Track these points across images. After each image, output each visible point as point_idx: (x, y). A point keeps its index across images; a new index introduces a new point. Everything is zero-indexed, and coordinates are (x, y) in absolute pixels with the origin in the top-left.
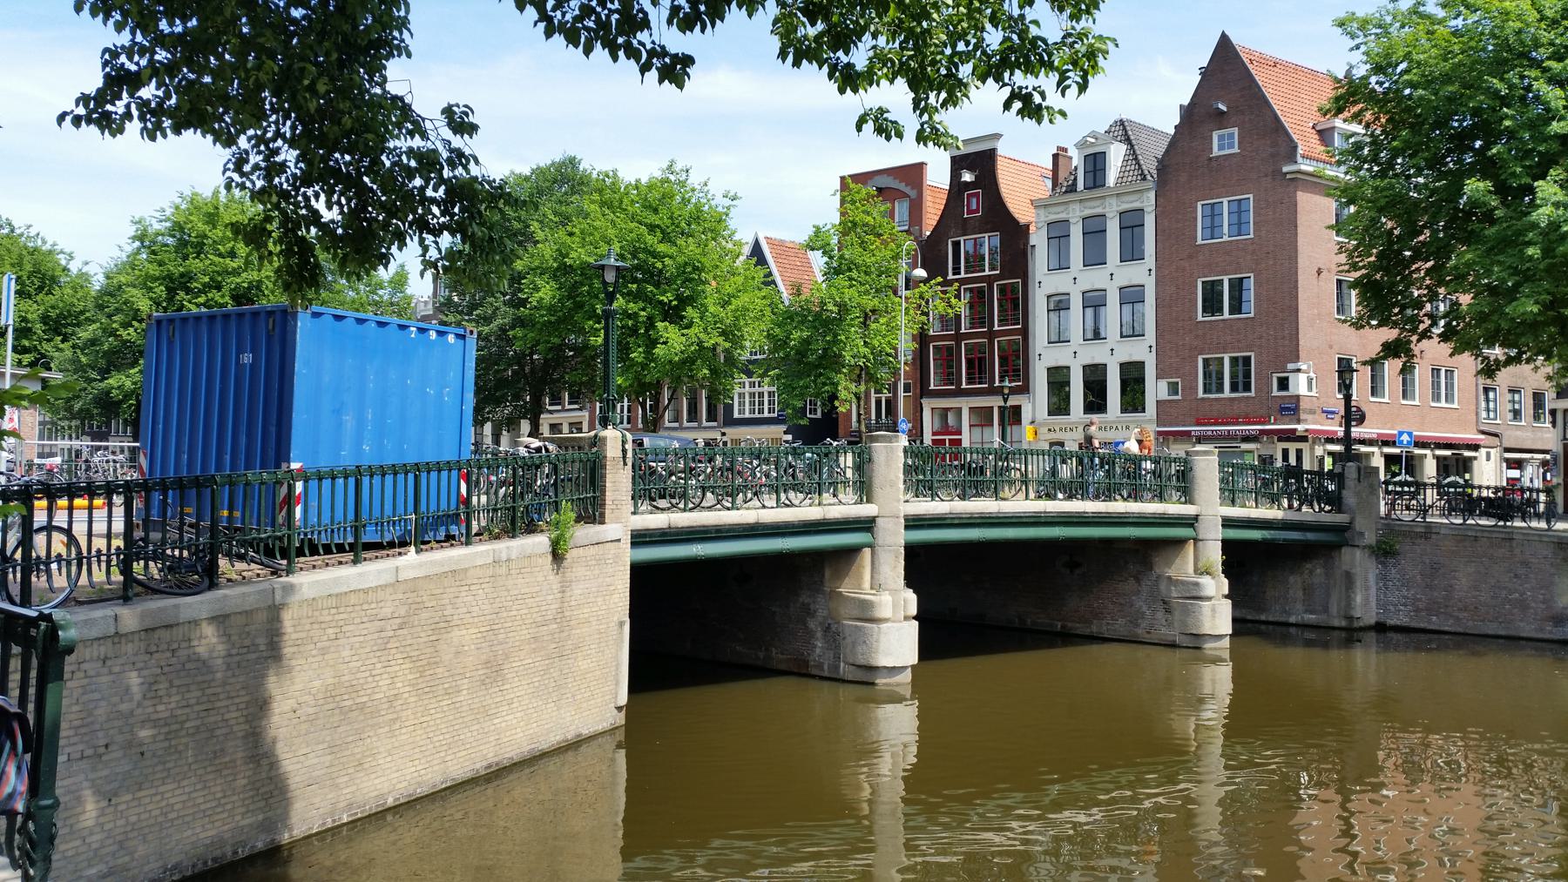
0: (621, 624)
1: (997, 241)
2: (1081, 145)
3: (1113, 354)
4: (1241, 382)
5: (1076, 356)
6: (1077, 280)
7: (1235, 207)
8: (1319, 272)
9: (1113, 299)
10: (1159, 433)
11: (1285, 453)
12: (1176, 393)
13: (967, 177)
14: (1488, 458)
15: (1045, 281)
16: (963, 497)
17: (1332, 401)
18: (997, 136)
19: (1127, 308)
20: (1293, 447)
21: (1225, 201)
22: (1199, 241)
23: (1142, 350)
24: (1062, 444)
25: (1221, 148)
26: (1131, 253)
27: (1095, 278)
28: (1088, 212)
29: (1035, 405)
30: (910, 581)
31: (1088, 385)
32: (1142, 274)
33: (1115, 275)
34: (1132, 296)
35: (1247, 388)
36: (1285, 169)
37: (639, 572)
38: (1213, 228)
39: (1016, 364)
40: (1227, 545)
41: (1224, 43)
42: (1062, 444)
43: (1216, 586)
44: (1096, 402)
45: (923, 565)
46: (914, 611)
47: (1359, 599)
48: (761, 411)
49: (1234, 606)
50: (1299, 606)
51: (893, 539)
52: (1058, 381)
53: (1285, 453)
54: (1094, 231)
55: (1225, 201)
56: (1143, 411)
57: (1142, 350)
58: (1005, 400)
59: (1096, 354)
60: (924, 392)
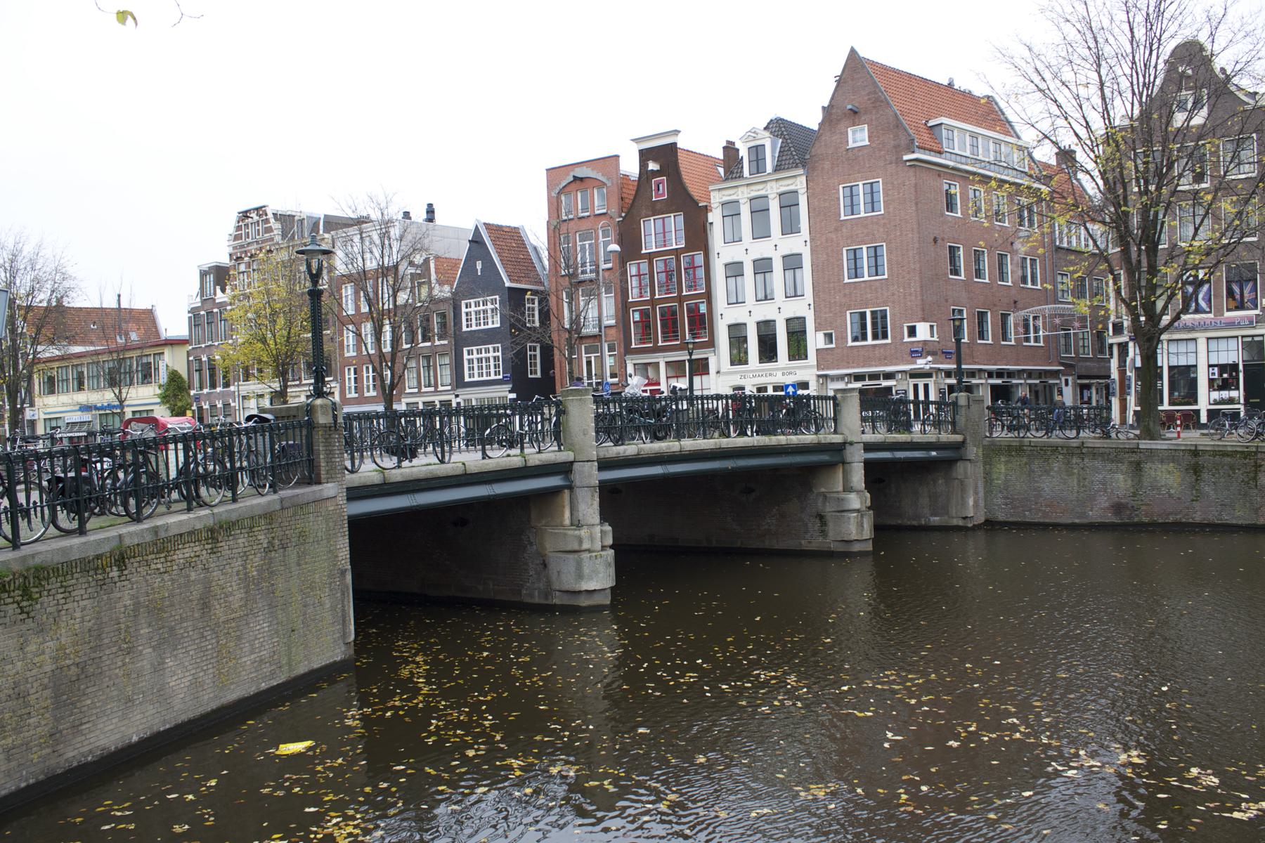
0: (343, 573)
1: (681, 219)
2: (745, 139)
3: (780, 311)
4: (880, 333)
5: (750, 314)
6: (748, 250)
7: (848, 191)
8: (935, 240)
9: (778, 265)
10: (819, 376)
11: (916, 386)
12: (885, 336)
13: (653, 166)
14: (1067, 384)
15: (722, 252)
16: (656, 438)
17: (950, 344)
18: (676, 132)
19: (789, 274)
20: (921, 383)
21: (861, 184)
22: (843, 218)
23: (802, 308)
24: (743, 388)
25: (854, 142)
26: (790, 227)
27: (762, 249)
28: (783, 189)
29: (720, 357)
30: (605, 516)
31: (791, 334)
32: (799, 244)
33: (778, 246)
34: (792, 262)
35: (885, 336)
36: (906, 158)
37: (358, 526)
38: (852, 208)
39: (702, 322)
40: (868, 464)
41: (853, 52)
42: (743, 388)
43: (857, 501)
44: (768, 351)
45: (614, 498)
46: (610, 541)
47: (971, 502)
48: (489, 374)
49: (876, 516)
50: (926, 511)
51: (588, 475)
52: (737, 335)
53: (916, 386)
54: (760, 211)
55: (861, 184)
56: (806, 358)
57: (802, 308)
58: (691, 354)
59: (766, 312)
60: (628, 351)
